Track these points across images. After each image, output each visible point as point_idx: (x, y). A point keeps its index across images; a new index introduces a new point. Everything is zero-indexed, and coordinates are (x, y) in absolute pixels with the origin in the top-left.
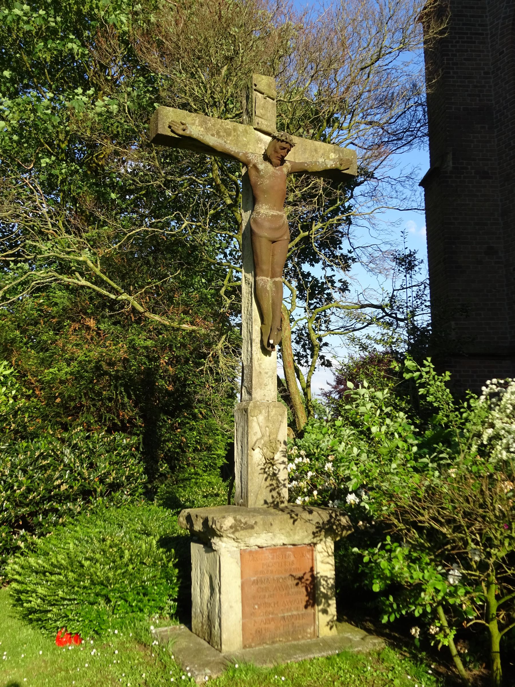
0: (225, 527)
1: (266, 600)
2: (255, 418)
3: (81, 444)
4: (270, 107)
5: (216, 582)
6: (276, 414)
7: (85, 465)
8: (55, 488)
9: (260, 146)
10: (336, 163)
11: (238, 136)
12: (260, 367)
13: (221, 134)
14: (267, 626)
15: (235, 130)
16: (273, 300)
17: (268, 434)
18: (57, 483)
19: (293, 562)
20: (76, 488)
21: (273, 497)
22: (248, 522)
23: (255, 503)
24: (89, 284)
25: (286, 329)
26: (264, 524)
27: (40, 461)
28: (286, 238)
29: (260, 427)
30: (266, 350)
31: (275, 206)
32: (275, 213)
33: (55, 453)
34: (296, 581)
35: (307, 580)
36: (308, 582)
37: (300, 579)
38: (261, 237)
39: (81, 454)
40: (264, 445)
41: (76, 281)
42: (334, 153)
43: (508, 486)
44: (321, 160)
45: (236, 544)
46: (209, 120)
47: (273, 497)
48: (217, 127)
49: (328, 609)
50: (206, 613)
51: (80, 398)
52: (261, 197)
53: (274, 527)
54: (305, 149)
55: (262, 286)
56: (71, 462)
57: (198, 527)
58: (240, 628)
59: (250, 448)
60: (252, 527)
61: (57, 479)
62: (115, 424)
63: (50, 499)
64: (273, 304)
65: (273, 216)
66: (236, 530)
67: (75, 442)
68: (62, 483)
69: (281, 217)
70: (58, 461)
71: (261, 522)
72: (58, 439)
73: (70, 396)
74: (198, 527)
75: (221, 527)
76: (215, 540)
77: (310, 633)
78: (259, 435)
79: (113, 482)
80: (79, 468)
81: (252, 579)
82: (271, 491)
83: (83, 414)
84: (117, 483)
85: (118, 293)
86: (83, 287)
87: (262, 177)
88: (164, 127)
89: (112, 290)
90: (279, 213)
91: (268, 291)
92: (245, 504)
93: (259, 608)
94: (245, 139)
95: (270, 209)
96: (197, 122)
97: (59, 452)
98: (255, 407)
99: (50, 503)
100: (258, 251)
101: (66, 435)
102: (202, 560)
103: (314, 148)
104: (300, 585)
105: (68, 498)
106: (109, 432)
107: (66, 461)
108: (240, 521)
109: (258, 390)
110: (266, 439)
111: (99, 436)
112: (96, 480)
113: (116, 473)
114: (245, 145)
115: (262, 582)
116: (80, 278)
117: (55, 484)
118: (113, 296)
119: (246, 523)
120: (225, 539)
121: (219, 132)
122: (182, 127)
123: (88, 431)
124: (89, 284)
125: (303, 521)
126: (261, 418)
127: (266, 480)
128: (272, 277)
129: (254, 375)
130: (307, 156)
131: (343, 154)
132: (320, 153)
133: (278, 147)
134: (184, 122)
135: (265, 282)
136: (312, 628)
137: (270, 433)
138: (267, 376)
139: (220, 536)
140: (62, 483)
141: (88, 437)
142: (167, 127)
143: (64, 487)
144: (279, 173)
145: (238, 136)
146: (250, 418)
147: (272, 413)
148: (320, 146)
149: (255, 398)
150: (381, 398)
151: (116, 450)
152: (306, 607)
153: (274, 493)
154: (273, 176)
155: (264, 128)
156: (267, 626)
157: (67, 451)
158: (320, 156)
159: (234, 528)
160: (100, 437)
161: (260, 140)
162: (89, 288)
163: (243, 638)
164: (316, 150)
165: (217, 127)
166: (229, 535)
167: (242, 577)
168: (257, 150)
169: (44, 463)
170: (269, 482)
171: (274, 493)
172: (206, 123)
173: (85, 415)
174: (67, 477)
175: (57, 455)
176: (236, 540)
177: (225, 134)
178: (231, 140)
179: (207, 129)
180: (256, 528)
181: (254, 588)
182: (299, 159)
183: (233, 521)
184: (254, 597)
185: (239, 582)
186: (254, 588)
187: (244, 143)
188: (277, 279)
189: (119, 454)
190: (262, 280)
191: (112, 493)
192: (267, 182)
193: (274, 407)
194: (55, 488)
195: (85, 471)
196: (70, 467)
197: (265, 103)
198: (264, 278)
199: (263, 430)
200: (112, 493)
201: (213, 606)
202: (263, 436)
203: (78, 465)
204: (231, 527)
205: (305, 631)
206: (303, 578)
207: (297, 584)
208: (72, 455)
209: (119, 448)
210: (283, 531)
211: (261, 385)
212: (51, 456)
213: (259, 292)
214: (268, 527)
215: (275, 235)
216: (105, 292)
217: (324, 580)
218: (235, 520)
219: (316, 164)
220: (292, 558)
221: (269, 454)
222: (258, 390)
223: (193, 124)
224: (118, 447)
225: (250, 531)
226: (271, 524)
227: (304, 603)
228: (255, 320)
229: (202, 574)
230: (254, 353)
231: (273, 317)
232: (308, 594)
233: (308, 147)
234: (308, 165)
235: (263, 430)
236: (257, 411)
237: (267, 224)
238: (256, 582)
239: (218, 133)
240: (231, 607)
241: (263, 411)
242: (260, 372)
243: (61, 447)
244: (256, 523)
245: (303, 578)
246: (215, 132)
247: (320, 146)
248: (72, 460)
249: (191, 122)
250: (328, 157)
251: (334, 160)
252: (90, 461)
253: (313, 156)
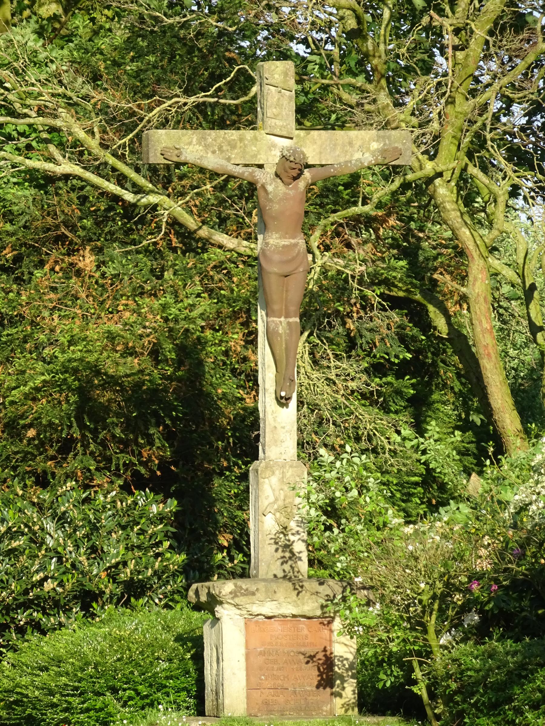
0: (224, 593)
1: (275, 673)
2: (266, 480)
3: (74, 513)
4: (285, 102)
5: (220, 651)
6: (292, 475)
7: (82, 551)
8: (34, 586)
9: (273, 153)
10: (377, 158)
11: (245, 146)
12: (275, 421)
13: (225, 148)
14: (275, 698)
15: (241, 140)
16: (286, 344)
17: (282, 498)
18: (37, 578)
19: (306, 636)
20: (68, 586)
21: (284, 571)
22: (250, 589)
23: (267, 573)
24: (77, 170)
25: (475, 280)
26: (267, 591)
27: (7, 542)
28: (301, 270)
29: (273, 490)
30: (283, 401)
31: (287, 233)
32: (286, 242)
33: (29, 527)
34: (306, 660)
35: (320, 659)
36: (321, 662)
37: (312, 657)
38: (270, 273)
39: (75, 531)
40: (277, 510)
41: (49, 166)
42: (377, 141)
43: (543, 561)
44: (358, 155)
45: (238, 612)
46: (209, 135)
47: (284, 571)
48: (219, 141)
49: (343, 693)
50: (214, 689)
51: (70, 427)
52: (271, 223)
53: (278, 595)
54: (335, 145)
55: (274, 329)
56: (59, 545)
57: (203, 598)
58: (245, 695)
59: (260, 513)
60: (253, 594)
61: (37, 572)
62: (136, 474)
63: (26, 605)
64: (287, 349)
65: (284, 246)
66: (236, 596)
67: (63, 509)
68: (45, 579)
69: (296, 245)
70: (35, 543)
71: (264, 589)
72: (33, 504)
73: (51, 424)
74: (203, 598)
75: (220, 592)
76: (218, 608)
77: (326, 711)
78: (272, 499)
79: (132, 579)
80: (73, 555)
81: (259, 650)
82: (282, 564)
83: (76, 455)
84: (139, 581)
85: (138, 190)
86: (66, 177)
87: (271, 201)
88: (156, 155)
89: (138, 190)
90: (293, 241)
91: (280, 335)
92: (256, 576)
93: (266, 679)
94: (254, 149)
95: (280, 238)
96: (194, 140)
97: (36, 528)
98: (266, 467)
99: (28, 612)
100: (267, 289)
101: (46, 496)
102: (211, 634)
103: (347, 141)
104: (310, 664)
105: (57, 604)
106: (126, 489)
107: (50, 542)
108: (241, 588)
109: (273, 447)
110: (280, 503)
111: (106, 497)
112: (103, 575)
113: (137, 564)
114: (255, 156)
115: (270, 654)
116: (59, 157)
117: (34, 579)
118: (129, 197)
119: (247, 590)
120: (226, 606)
121: (222, 147)
122: (176, 152)
123: (86, 487)
124: (77, 170)
125: (308, 594)
126: (274, 480)
127: (277, 550)
128: (286, 317)
129: (267, 430)
130: (337, 153)
131: (389, 139)
132: (357, 147)
133: (287, 167)
134: (178, 147)
135: (276, 324)
136: (329, 706)
137: (286, 496)
138: (284, 430)
139: (221, 603)
140: (45, 579)
141: (87, 500)
142: (159, 154)
143: (49, 585)
144: (291, 193)
145: (245, 146)
146: (261, 480)
147: (288, 475)
148: (357, 137)
149: (269, 457)
150: (359, 463)
151: (138, 524)
152: (318, 687)
153: (287, 567)
154: (286, 198)
155: (278, 132)
156: (275, 698)
157: (50, 526)
158: (356, 149)
159: (234, 594)
160: (108, 500)
161: (274, 146)
162: (76, 177)
163: (247, 704)
164: (351, 144)
165: (219, 141)
166: (229, 601)
167: (247, 647)
168: (270, 159)
169: (15, 544)
170: (280, 554)
171: (287, 567)
172: (205, 139)
173: (79, 457)
174: (52, 568)
175: (35, 533)
176: (236, 606)
177: (229, 148)
178: (237, 154)
179: (207, 147)
180: (258, 595)
181: (261, 659)
182: (327, 160)
183: (233, 587)
184: (261, 669)
185: (243, 651)
186: (261, 659)
187: (252, 154)
188: (291, 320)
189: (142, 532)
190: (273, 321)
191: (132, 600)
192: (276, 207)
193: (291, 466)
194: (34, 586)
195: (83, 558)
196: (57, 552)
197: (279, 99)
198: (275, 319)
199: (277, 493)
200: (132, 600)
201: (218, 679)
202: (276, 500)
203: (71, 549)
204: (231, 593)
205: (320, 708)
206: (314, 656)
207: (308, 662)
208: (59, 532)
209: (143, 520)
210: (289, 600)
211: (276, 441)
212: (23, 534)
213: (270, 335)
214: (272, 596)
215: (287, 269)
216: (113, 188)
217: (339, 660)
218: (236, 585)
219: (346, 166)
220: (305, 632)
221: (283, 520)
222: (273, 447)
223: (190, 143)
224: (141, 518)
225: (250, 597)
226: (275, 592)
227: (316, 683)
228: (269, 366)
229: (211, 649)
230: (267, 405)
231: (287, 365)
232: (321, 674)
233: (340, 142)
234: (335, 169)
235: (277, 493)
236: (268, 473)
237: (276, 257)
238: (262, 653)
239: (220, 148)
240: (234, 674)
241: (277, 472)
242: (275, 427)
243: (40, 519)
244: (257, 590)
245: (314, 656)
246: (216, 148)
247: (357, 137)
248: (61, 541)
249: (187, 141)
250: (368, 149)
251: (373, 154)
252: (91, 543)
253: (347, 151)
